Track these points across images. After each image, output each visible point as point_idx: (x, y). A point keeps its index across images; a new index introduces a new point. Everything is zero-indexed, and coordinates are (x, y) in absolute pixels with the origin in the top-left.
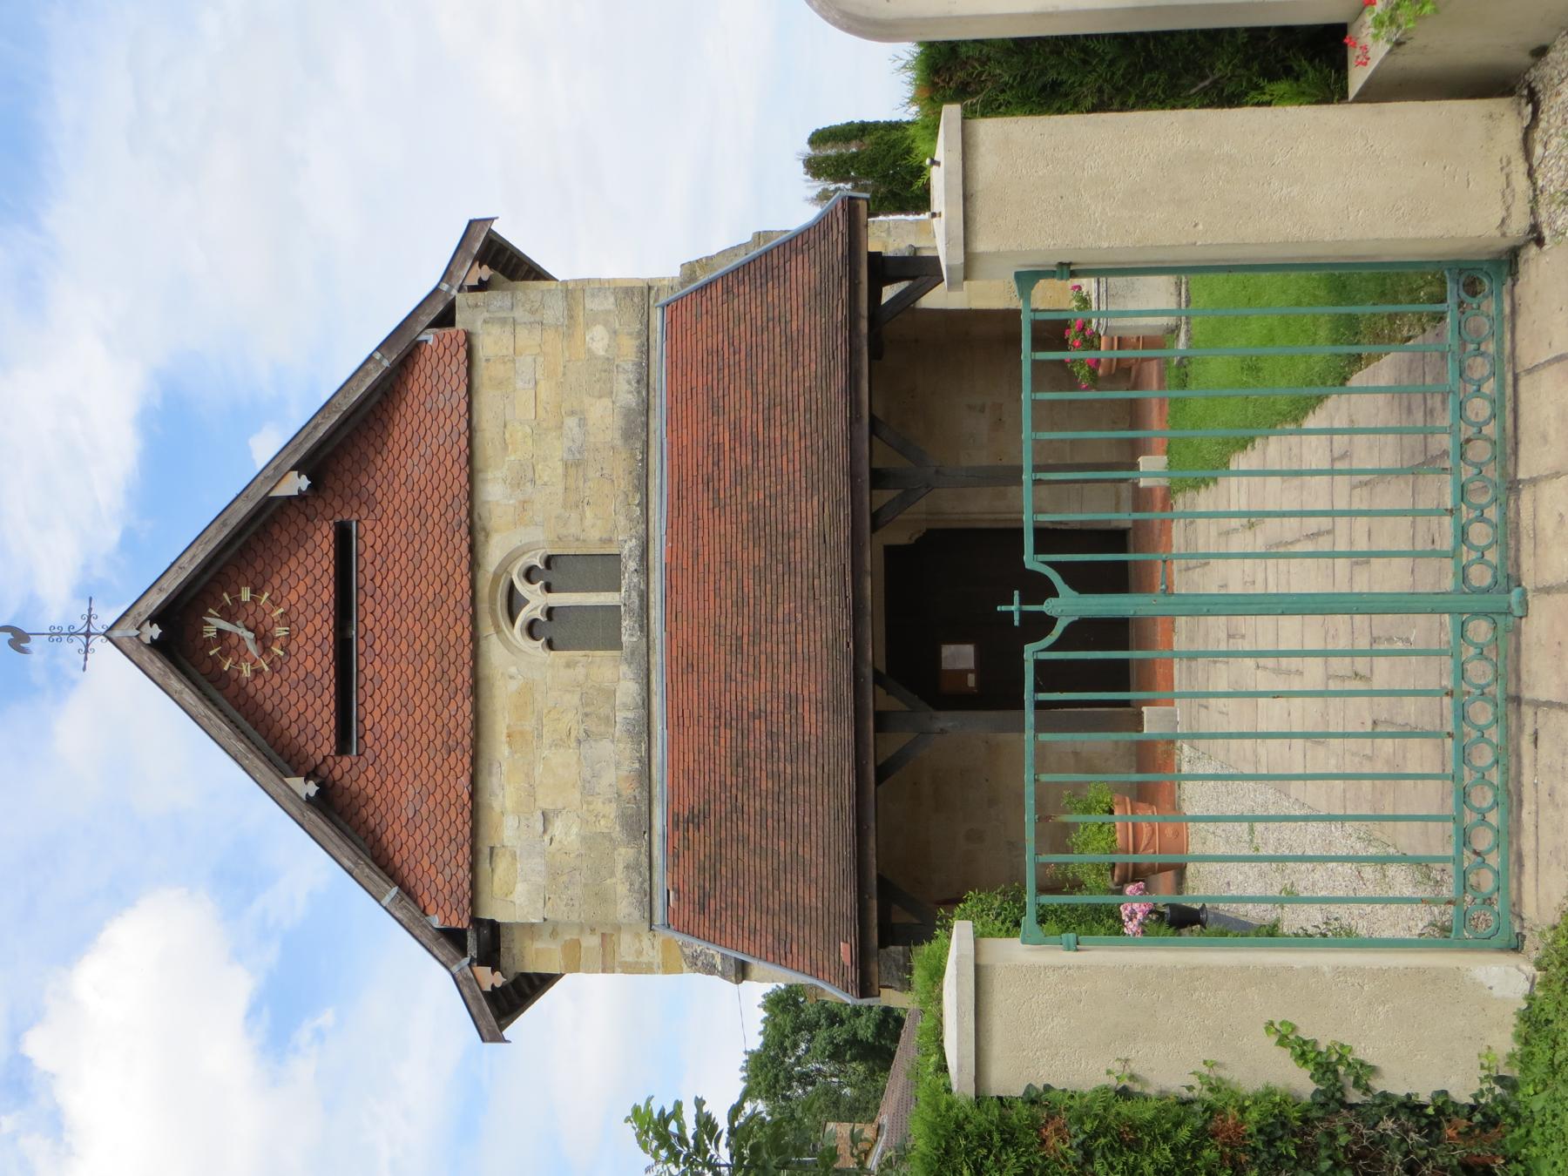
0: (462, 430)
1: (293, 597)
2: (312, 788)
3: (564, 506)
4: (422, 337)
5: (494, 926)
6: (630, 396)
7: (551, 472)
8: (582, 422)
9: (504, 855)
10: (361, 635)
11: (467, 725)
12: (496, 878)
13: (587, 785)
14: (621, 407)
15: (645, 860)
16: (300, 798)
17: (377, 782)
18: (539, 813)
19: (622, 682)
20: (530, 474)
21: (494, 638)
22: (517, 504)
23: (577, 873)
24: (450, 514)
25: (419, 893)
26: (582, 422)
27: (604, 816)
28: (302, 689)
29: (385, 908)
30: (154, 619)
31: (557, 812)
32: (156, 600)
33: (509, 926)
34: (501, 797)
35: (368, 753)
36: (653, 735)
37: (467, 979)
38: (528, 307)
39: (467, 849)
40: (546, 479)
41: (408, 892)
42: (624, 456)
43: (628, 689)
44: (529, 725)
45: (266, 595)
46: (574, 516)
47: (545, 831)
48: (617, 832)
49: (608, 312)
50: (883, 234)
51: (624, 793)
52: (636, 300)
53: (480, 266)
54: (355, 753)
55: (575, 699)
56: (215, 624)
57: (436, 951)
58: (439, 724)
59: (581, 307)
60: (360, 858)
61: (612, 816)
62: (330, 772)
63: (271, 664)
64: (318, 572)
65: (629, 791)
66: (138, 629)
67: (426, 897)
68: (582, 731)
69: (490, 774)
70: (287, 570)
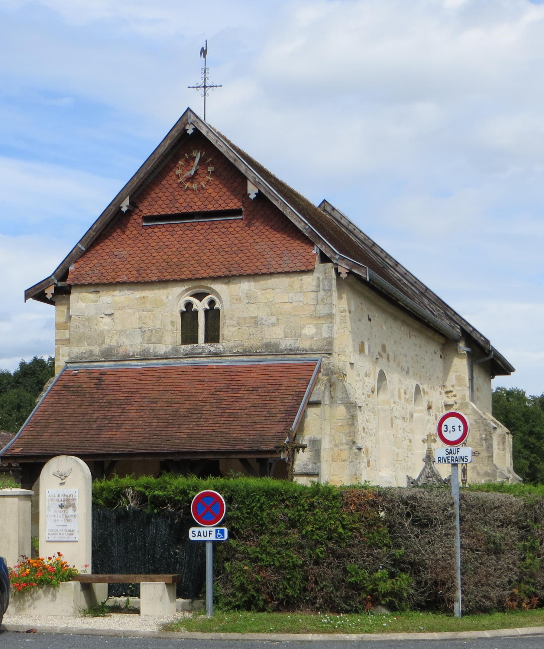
0: (270, 270)
1: (210, 191)
2: (124, 209)
3: (238, 318)
4: (315, 247)
5: (69, 293)
6: (284, 346)
7: (253, 311)
8: (274, 324)
9: (97, 297)
10: (193, 224)
11: (147, 279)
12: (87, 294)
13: (124, 332)
14: (280, 342)
15: (94, 359)
16: (120, 204)
17: (131, 236)
18: (113, 312)
19: (165, 346)
20: (252, 301)
21: (184, 288)
22: (239, 296)
23: (89, 330)
24: (235, 266)
25: (84, 259)
26: (274, 324)
27: (111, 340)
28: (171, 198)
29: (76, 245)
30: (196, 130)
31: (113, 320)
32: (204, 131)
33: (68, 300)
34: (120, 294)
35: (144, 230)
36: (142, 361)
37: (49, 282)
38: (325, 297)
39: (98, 281)
40: (250, 309)
41: (83, 254)
42: (258, 344)
43: (162, 349)
44: (148, 306)
45: (211, 179)
46: (234, 322)
47: (105, 315)
48: (105, 346)
49: (321, 335)
50: (350, 460)
51: (120, 349)
52: (326, 347)
53: (347, 273)
54: (144, 224)
55: (158, 326)
56: (197, 154)
57: (60, 268)
58: (150, 265)
59: (324, 322)
60: (97, 232)
61: (111, 344)
62: (136, 214)
63: (181, 183)
64: (220, 202)
65: (121, 351)
66: (191, 123)
67: (82, 262)
68: (145, 329)
69: (128, 290)
70: (221, 187)
